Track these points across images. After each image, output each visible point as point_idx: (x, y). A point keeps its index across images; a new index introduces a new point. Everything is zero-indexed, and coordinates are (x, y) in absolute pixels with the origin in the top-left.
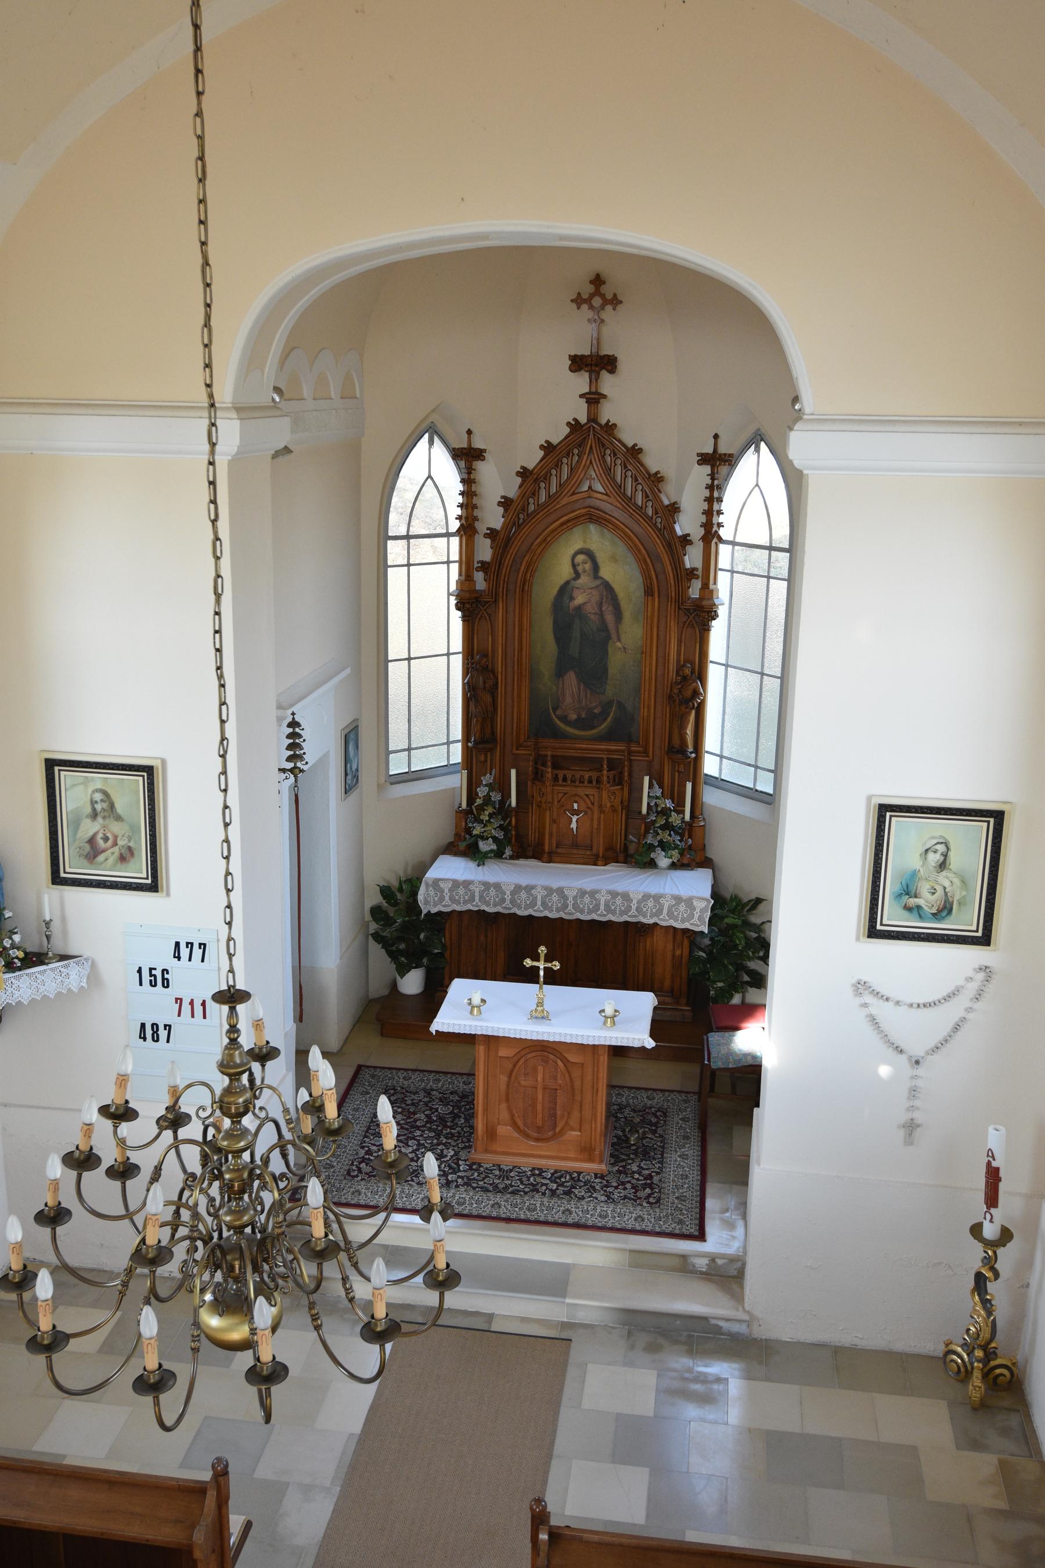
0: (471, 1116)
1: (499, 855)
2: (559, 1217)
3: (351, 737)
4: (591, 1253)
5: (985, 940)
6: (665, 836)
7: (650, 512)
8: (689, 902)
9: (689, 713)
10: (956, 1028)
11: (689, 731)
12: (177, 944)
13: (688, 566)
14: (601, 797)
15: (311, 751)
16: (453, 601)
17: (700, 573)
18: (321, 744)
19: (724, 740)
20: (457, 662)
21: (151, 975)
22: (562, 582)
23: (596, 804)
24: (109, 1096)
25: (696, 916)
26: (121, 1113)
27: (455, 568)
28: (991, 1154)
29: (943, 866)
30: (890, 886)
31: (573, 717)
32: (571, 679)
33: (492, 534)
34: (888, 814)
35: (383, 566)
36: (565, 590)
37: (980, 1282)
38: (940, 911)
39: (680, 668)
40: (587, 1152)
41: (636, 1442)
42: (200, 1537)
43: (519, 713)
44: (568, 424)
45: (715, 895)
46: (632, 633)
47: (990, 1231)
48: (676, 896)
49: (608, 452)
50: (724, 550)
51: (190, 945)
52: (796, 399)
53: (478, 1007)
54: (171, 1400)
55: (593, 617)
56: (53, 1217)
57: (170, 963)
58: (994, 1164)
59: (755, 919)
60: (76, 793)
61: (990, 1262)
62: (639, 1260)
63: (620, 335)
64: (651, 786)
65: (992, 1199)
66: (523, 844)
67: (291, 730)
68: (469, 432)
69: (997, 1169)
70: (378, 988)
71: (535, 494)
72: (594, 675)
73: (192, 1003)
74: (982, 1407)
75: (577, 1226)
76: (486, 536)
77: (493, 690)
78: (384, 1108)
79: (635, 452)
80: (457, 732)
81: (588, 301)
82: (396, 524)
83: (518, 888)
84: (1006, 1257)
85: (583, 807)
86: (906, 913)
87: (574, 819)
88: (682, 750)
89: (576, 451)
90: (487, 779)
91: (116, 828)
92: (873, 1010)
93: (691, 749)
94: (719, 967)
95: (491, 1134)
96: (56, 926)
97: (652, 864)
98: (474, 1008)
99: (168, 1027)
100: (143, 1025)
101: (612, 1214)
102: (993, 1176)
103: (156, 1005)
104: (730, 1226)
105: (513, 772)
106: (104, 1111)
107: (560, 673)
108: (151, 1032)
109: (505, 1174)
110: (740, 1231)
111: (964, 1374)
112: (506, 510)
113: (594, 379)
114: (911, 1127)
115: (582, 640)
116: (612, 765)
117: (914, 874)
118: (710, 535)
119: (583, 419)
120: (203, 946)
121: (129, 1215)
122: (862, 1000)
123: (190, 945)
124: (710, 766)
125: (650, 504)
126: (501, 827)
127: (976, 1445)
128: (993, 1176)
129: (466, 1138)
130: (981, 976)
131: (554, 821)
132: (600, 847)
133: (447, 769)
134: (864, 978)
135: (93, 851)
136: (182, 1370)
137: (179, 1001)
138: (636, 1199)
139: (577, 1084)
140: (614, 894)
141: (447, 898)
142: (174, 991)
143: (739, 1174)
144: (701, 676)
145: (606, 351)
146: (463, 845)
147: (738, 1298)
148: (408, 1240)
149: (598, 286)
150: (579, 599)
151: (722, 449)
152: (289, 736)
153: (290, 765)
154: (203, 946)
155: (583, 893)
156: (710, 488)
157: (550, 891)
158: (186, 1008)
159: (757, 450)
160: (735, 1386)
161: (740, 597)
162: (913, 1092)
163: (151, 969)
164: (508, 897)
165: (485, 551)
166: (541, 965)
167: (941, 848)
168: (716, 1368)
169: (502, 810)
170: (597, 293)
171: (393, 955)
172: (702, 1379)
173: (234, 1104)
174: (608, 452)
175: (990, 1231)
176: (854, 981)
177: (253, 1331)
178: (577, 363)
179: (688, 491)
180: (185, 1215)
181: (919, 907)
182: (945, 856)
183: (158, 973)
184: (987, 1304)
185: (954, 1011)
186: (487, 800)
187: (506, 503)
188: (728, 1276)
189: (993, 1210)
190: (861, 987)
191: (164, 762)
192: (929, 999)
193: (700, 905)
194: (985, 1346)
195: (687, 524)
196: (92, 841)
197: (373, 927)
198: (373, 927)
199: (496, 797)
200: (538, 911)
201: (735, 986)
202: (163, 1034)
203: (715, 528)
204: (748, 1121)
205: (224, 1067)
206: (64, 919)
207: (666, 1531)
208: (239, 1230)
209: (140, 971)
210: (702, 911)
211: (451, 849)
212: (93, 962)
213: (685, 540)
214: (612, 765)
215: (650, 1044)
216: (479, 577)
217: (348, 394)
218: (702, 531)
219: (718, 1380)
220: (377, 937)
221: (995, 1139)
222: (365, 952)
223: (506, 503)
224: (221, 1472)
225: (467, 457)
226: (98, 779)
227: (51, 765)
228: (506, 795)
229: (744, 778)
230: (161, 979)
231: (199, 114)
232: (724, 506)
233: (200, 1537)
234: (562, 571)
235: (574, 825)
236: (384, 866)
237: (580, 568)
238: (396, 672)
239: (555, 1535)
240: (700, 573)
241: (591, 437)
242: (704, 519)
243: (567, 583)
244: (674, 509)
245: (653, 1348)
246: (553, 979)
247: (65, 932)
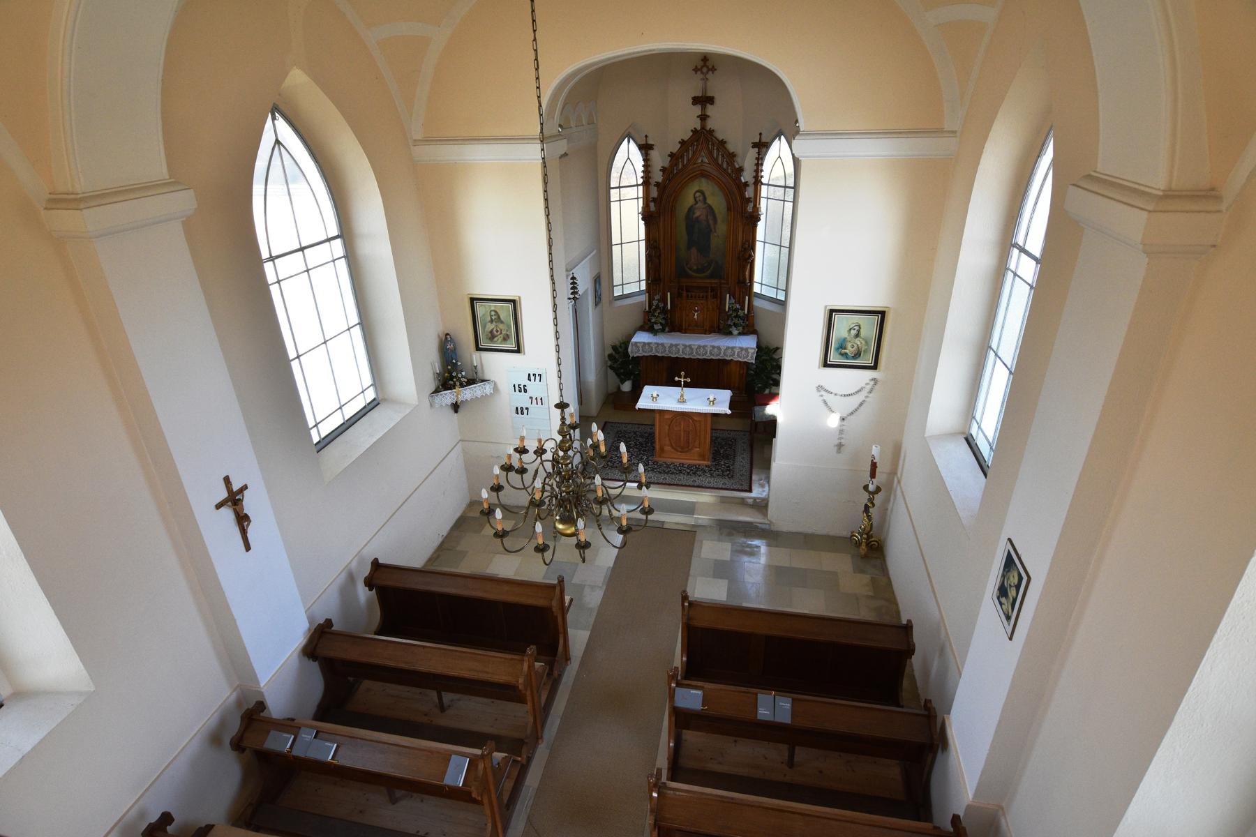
0: (653, 443)
1: (663, 331)
2: (691, 483)
3: (597, 280)
4: (704, 498)
5: (875, 367)
6: (736, 321)
8: (746, 350)
10: (861, 405)
15: (581, 289)
18: (584, 285)
19: (763, 278)
20: (643, 244)
24: (517, 444)
26: (522, 451)
27: (641, 201)
28: (873, 457)
29: (857, 335)
32: (694, 250)
33: (658, 185)
35: (609, 202)
36: (691, 210)
37: (867, 508)
39: (743, 244)
40: (703, 457)
41: (722, 570)
42: (554, 603)
45: (758, 346)
47: (871, 488)
48: (743, 346)
50: (764, 188)
52: (797, 121)
53: (656, 398)
54: (548, 555)
56: (497, 489)
57: (526, 382)
59: (776, 357)
60: (481, 309)
61: (871, 501)
62: (724, 500)
63: (716, 86)
65: (873, 475)
66: (673, 326)
70: (612, 389)
74: (866, 557)
75: (698, 487)
78: (623, 447)
79: (723, 143)
80: (643, 276)
81: (701, 70)
82: (614, 183)
83: (671, 345)
84: (878, 499)
88: (744, 282)
90: (657, 297)
91: (501, 326)
94: (761, 377)
95: (662, 450)
96: (479, 368)
97: (730, 333)
98: (654, 398)
101: (713, 482)
102: (874, 465)
103: (522, 400)
104: (763, 486)
106: (516, 450)
107: (689, 248)
108: (520, 411)
109: (668, 466)
110: (766, 489)
111: (858, 544)
113: (704, 108)
114: (840, 446)
115: (699, 232)
116: (713, 289)
117: (845, 339)
118: (758, 182)
121: (525, 488)
124: (757, 288)
127: (862, 572)
128: (874, 465)
129: (652, 451)
135: (492, 337)
136: (551, 544)
138: (723, 476)
140: (713, 347)
142: (529, 394)
143: (766, 465)
144: (753, 248)
145: (709, 94)
146: (647, 327)
147: (765, 515)
148: (633, 494)
149: (705, 64)
150: (697, 214)
151: (764, 140)
155: (699, 347)
156: (758, 159)
157: (685, 346)
160: (763, 549)
161: (771, 207)
162: (841, 432)
165: (654, 193)
168: (756, 542)
169: (664, 311)
170: (705, 65)
171: (618, 375)
172: (750, 546)
173: (564, 445)
175: (871, 488)
177: (577, 530)
178: (696, 101)
180: (547, 488)
184: (869, 517)
186: (657, 306)
187: (663, 170)
188: (761, 506)
190: (820, 388)
193: (751, 351)
194: (868, 533)
195: (747, 177)
196: (491, 332)
197: (609, 363)
198: (609, 363)
199: (661, 305)
200: (681, 355)
201: (767, 386)
204: (770, 443)
205: (560, 432)
207: (735, 603)
208: (568, 493)
211: (642, 328)
213: (746, 184)
214: (713, 289)
215: (729, 412)
216: (652, 205)
217: (591, 123)
219: (758, 547)
220: (611, 367)
221: (875, 450)
222: (606, 373)
223: (663, 170)
224: (561, 581)
225: (645, 148)
226: (493, 305)
227: (472, 300)
229: (771, 293)
231: (535, 40)
233: (554, 603)
234: (689, 201)
236: (613, 337)
238: (616, 250)
239: (691, 604)
241: (703, 137)
244: (741, 170)
245: (730, 534)
246: (687, 385)
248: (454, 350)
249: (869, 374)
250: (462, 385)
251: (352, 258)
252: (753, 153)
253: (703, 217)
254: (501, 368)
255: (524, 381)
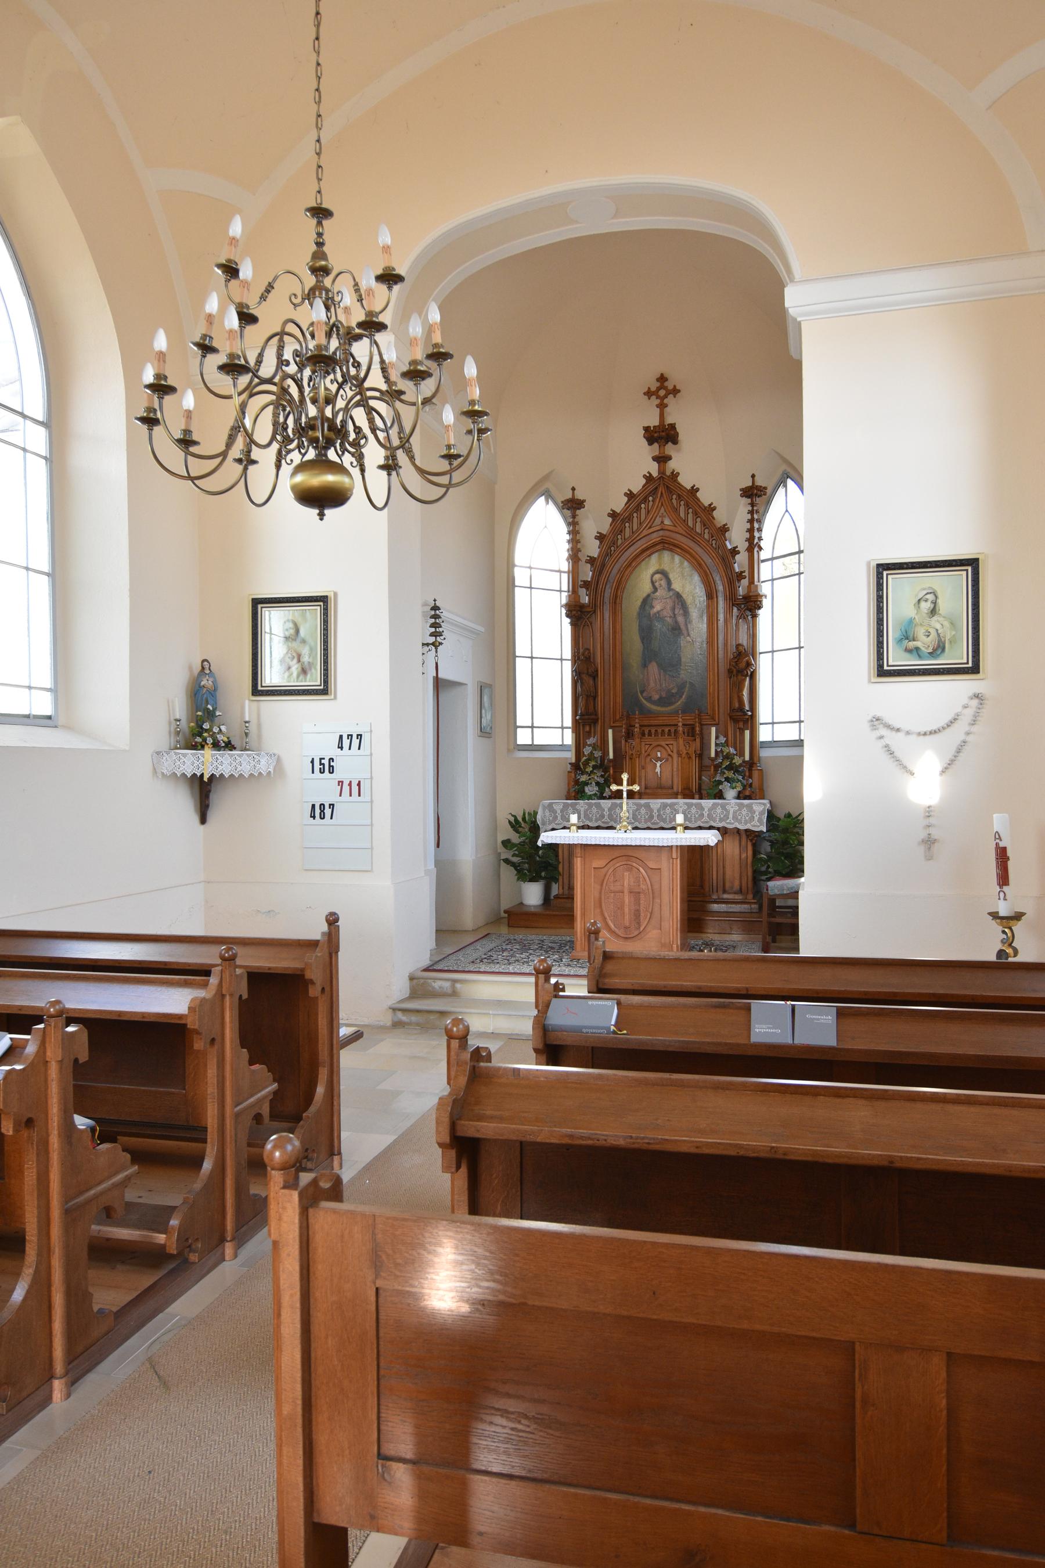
5: (975, 669)
6: (730, 774)
7: (706, 536)
9: (744, 680)
10: (959, 751)
11: (745, 693)
12: (341, 737)
13: (737, 570)
14: (678, 744)
16: (564, 611)
17: (746, 574)
20: (568, 666)
21: (321, 764)
22: (645, 595)
23: (675, 751)
25: (756, 819)
28: (998, 836)
29: (933, 612)
30: (892, 634)
31: (656, 697)
32: (653, 668)
33: (591, 561)
34: (885, 573)
35: (532, 748)
36: (647, 601)
38: (935, 650)
43: (615, 703)
44: (644, 476)
46: (699, 627)
49: (674, 497)
51: (350, 736)
55: (668, 619)
58: (1001, 845)
64: (717, 738)
67: (433, 630)
68: (573, 489)
69: (1005, 848)
71: (621, 531)
72: (671, 665)
73: (350, 784)
76: (587, 562)
77: (594, 676)
85: (665, 755)
86: (907, 655)
87: (658, 764)
88: (741, 708)
89: (651, 498)
92: (887, 741)
93: (747, 708)
96: (253, 728)
99: (332, 806)
100: (313, 806)
102: (1002, 856)
103: (324, 789)
105: (610, 731)
108: (319, 811)
112: (601, 543)
114: (929, 842)
117: (911, 621)
118: (753, 545)
119: (655, 474)
120: (359, 736)
122: (878, 733)
123: (350, 736)
125: (706, 531)
126: (602, 776)
128: (1002, 856)
130: (975, 703)
131: (643, 768)
132: (678, 786)
133: (562, 747)
134: (878, 714)
137: (341, 783)
139: (656, 887)
141: (559, 818)
142: (338, 775)
150: (658, 607)
152: (432, 617)
153: (432, 639)
154: (359, 736)
156: (751, 521)
158: (346, 788)
159: (785, 486)
163: (321, 759)
164: (606, 813)
166: (625, 788)
167: (931, 597)
174: (674, 497)
176: (870, 718)
179: (733, 514)
181: (917, 649)
182: (935, 603)
183: (326, 762)
185: (957, 734)
186: (591, 757)
187: (601, 537)
189: (1005, 888)
190: (876, 721)
191: (335, 594)
192: (935, 727)
195: (737, 538)
202: (328, 811)
203: (756, 541)
206: (259, 725)
209: (312, 762)
210: (761, 813)
212: (279, 760)
213: (734, 552)
216: (583, 592)
218: (747, 544)
221: (999, 822)
225: (572, 507)
228: (605, 752)
230: (327, 766)
232: (764, 534)
235: (658, 770)
236: (512, 803)
237: (657, 584)
240: (746, 574)
241: (663, 487)
242: (747, 535)
243: (649, 596)
244: (724, 529)
247: (259, 736)
248: (213, 692)
249: (961, 687)
250: (216, 745)
251: (57, 461)
252: (743, 507)
253: (667, 613)
254: (297, 730)
255: (329, 750)
